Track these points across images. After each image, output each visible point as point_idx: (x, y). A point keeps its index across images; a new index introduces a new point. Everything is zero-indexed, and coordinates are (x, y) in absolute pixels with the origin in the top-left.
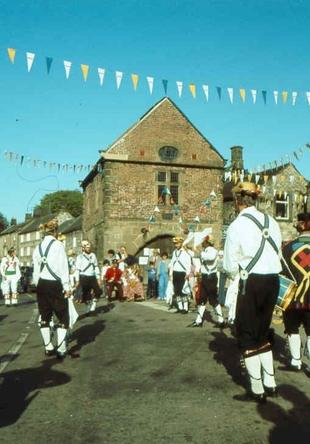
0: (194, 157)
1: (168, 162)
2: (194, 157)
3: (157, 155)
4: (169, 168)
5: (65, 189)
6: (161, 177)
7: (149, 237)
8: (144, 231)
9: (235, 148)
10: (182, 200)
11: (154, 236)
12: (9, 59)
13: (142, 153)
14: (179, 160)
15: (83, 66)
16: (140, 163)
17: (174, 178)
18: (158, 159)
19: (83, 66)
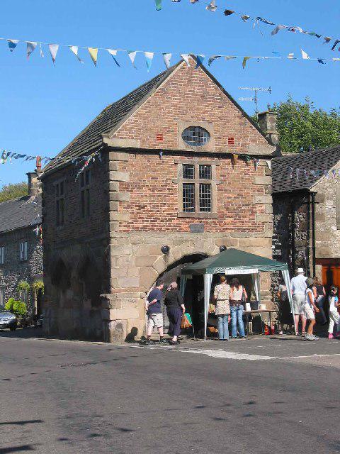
0: (231, 141)
1: (194, 149)
2: (231, 141)
3: (180, 139)
4: (196, 159)
5: (111, 103)
6: (188, 171)
7: (171, 260)
8: (166, 250)
9: (200, 175)
10: (216, 205)
11: (179, 256)
12: (46, 250)
13: (160, 137)
14: (211, 146)
15: (90, 49)
16: (156, 152)
17: (205, 173)
18: (182, 145)
19: (90, 49)
